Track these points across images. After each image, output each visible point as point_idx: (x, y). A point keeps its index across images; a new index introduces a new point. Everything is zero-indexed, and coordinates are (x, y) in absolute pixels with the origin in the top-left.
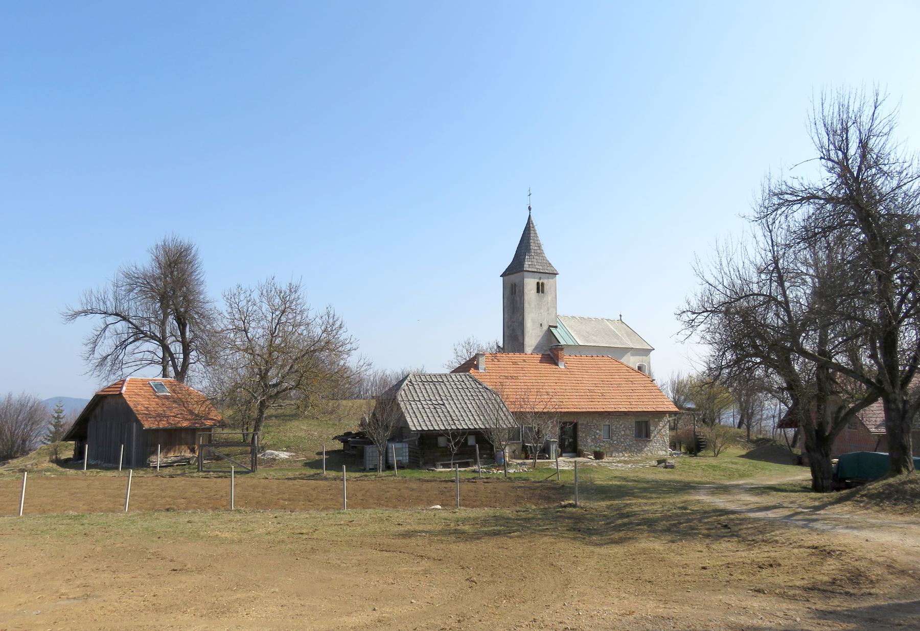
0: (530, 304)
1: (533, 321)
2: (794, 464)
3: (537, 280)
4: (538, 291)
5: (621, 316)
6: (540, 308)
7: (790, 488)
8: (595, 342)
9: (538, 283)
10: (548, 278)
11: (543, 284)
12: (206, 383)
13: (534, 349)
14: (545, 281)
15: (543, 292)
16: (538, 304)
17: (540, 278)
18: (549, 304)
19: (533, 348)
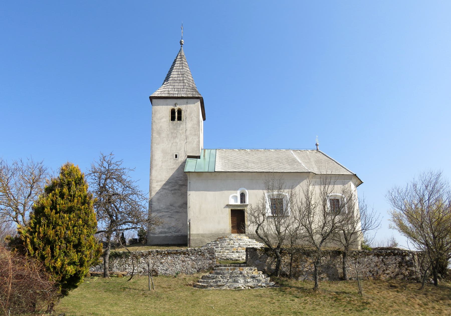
0: (159, 133)
1: (164, 152)
2: (186, 213)
3: (172, 107)
4: (173, 119)
5: (317, 145)
6: (175, 138)
7: (152, 163)
8: (247, 168)
9: (173, 112)
10: (187, 103)
11: (180, 112)
12: (58, 227)
13: (165, 185)
14: (183, 107)
15: (180, 119)
16: (172, 133)
17: (175, 105)
18: (188, 133)
19: (164, 183)
